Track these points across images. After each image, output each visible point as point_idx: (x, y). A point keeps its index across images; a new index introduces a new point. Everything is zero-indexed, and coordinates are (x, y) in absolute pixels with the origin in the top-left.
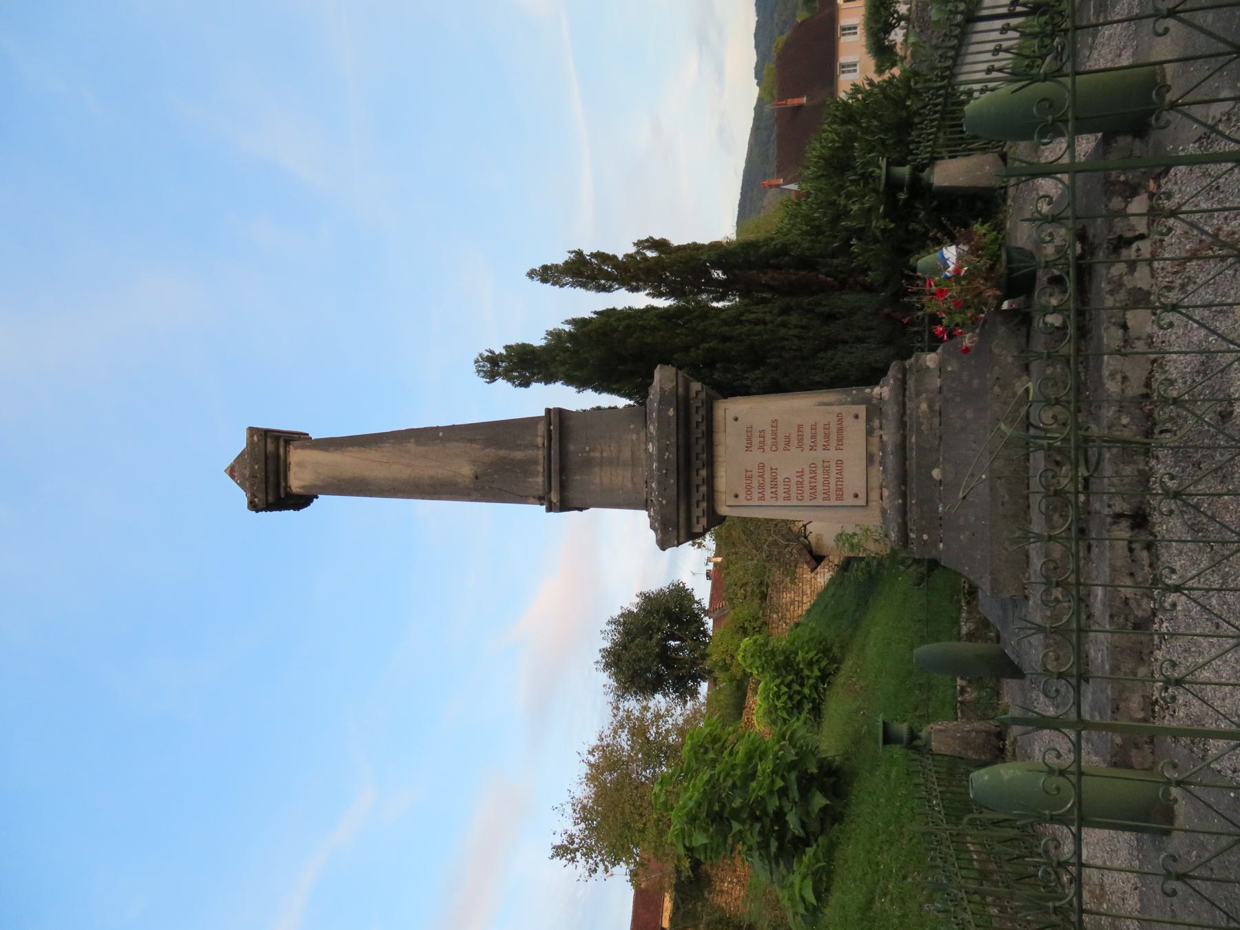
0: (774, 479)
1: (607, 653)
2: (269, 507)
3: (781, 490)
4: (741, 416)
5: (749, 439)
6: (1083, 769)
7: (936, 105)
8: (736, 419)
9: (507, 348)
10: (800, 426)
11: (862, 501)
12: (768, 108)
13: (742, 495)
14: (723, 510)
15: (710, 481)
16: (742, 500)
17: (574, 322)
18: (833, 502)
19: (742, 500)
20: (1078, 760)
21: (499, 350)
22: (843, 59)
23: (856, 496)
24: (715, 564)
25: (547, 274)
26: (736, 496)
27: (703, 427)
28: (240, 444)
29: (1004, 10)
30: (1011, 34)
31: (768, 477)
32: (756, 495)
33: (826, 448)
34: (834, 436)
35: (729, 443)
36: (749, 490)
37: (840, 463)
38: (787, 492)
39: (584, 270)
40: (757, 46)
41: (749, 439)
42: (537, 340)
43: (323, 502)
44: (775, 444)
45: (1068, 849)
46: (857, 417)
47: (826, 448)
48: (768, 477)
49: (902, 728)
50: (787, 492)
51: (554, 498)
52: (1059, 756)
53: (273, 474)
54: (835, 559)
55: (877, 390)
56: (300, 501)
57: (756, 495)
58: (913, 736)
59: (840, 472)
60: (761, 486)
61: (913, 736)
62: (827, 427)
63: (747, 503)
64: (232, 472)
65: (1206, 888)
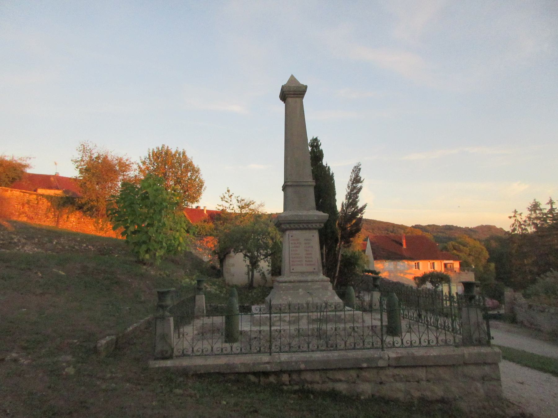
0: (297, 247)
1: (167, 153)
3: (294, 249)
4: (314, 237)
5: (307, 240)
9: (322, 151)
11: (292, 271)
12: (429, 236)
15: (296, 229)
16: (290, 238)
17: (333, 174)
19: (290, 238)
21: (321, 148)
22: (421, 263)
24: (203, 210)
25: (357, 170)
28: (302, 82)
31: (297, 245)
33: (306, 261)
34: (309, 263)
35: (306, 234)
36: (293, 240)
37: (302, 265)
39: (356, 180)
40: (429, 226)
41: (307, 240)
42: (325, 161)
43: (282, 105)
53: (292, 94)
55: (322, 274)
57: (292, 242)
65: (194, 344)
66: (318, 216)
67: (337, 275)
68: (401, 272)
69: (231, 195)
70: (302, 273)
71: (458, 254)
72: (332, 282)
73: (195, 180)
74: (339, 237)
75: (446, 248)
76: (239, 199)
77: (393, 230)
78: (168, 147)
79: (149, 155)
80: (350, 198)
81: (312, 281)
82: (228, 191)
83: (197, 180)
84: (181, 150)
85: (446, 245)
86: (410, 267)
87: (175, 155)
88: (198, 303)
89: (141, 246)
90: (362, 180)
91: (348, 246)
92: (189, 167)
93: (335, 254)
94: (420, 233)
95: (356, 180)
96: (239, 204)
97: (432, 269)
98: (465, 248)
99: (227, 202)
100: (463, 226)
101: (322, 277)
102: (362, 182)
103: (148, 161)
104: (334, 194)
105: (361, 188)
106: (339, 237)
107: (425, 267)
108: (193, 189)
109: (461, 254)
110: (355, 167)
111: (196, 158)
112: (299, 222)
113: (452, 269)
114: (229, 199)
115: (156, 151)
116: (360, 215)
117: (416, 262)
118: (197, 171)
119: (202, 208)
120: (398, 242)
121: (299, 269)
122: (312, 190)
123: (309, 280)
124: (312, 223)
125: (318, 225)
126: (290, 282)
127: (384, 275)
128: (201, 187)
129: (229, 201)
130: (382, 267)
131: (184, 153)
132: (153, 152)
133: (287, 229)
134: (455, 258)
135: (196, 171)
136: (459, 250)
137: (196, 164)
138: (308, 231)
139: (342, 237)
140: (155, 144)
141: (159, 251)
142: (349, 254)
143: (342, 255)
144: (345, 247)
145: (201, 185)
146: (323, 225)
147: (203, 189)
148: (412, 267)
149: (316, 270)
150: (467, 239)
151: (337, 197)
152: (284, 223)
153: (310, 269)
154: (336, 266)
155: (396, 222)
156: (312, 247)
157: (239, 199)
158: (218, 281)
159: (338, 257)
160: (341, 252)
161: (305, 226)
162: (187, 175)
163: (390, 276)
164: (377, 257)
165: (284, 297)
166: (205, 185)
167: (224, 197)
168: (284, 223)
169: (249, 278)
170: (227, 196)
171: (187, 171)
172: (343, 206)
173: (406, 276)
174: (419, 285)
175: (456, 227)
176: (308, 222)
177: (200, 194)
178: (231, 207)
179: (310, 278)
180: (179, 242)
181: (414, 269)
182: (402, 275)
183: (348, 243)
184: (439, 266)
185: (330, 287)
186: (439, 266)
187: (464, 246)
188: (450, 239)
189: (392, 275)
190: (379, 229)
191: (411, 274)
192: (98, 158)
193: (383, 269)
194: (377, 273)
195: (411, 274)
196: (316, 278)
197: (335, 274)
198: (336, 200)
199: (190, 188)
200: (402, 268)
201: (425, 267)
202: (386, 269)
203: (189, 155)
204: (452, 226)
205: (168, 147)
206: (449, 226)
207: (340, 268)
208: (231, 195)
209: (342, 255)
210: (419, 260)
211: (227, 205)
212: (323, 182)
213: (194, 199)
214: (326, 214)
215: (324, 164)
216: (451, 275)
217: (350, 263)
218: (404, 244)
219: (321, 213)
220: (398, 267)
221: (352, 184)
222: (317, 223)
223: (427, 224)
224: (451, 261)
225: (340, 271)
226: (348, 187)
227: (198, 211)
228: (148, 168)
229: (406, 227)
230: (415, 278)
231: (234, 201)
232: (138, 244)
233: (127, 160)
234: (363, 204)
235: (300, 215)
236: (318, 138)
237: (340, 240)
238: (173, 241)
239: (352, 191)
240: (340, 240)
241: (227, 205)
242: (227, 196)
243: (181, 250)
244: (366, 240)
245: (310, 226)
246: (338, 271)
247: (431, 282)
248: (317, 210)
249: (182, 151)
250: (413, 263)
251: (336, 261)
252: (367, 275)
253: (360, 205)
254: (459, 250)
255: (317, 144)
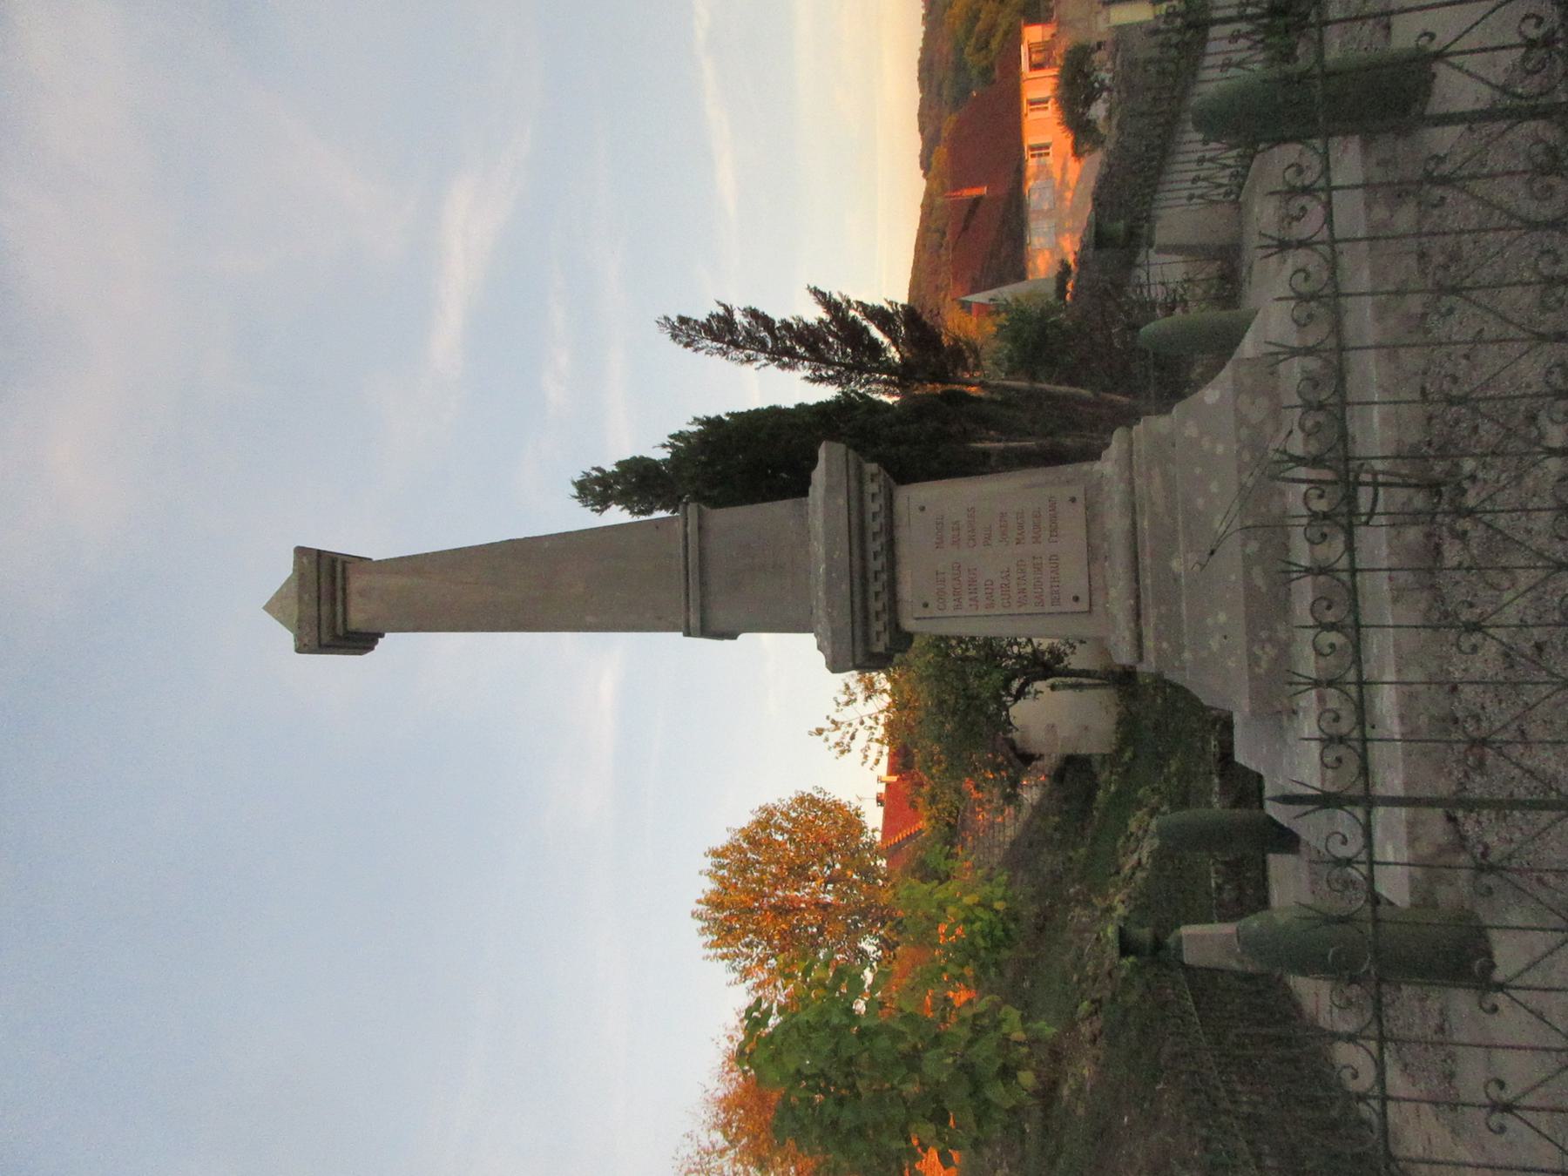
0: (972, 582)
1: (715, 903)
2: (323, 647)
3: (981, 595)
4: (928, 503)
6: (1390, 1092)
7: (1153, 159)
8: (923, 509)
9: (619, 464)
10: (1003, 515)
12: (949, 123)
13: (933, 604)
14: (909, 624)
15: (892, 585)
18: (1048, 608)
20: (1381, 1079)
21: (610, 467)
22: (1030, 139)
23: (1076, 599)
24: (888, 785)
25: (685, 331)
26: (926, 605)
27: (881, 519)
28: (285, 568)
29: (1232, 12)
30: (1243, 43)
31: (964, 578)
32: (950, 604)
37: (1054, 558)
38: (990, 596)
39: (726, 332)
40: (922, 130)
43: (391, 643)
44: (972, 538)
45: (1366, 1080)
46: (1073, 500)
47: (1037, 540)
48: (964, 578)
49: (1145, 934)
50: (990, 596)
51: (694, 621)
52: (1345, 842)
53: (336, 605)
54: (1049, 763)
55: (1097, 466)
56: (361, 642)
58: (1158, 945)
59: (1056, 569)
60: (956, 592)
61: (1158, 945)
62: (1037, 515)
63: (939, 614)
64: (268, 608)
66: (830, 489)
67: (1086, 393)
68: (1060, 197)
69: (833, 722)
70: (1093, 554)
71: (999, 35)
72: (1129, 418)
73: (794, 820)
74: (939, 389)
75: (986, 72)
76: (843, 699)
77: (938, 231)
78: (699, 902)
79: (724, 957)
80: (791, 353)
81: (1133, 509)
82: (820, 732)
83: (794, 815)
84: (708, 863)
85: (974, 72)
86: (1043, 170)
87: (722, 880)
88: (1214, 958)
89: (987, 1101)
90: (721, 311)
91: (975, 352)
92: (758, 836)
93: (1006, 403)
94: (942, 151)
95: (726, 332)
96: (861, 697)
97: (1049, 105)
98: (982, 16)
99: (853, 738)
100: (920, 31)
101: (1107, 466)
102: (729, 310)
103: (742, 963)
104: (775, 411)
105: (753, 314)
106: (939, 389)
107: (1043, 126)
108: (818, 829)
109: (1004, 25)
110: (674, 337)
111: (730, 817)
112: (861, 578)
113: (1046, 47)
114: (844, 728)
115: (710, 938)
116: (852, 313)
117: (1027, 154)
118: (770, 812)
119: (882, 788)
120: (971, 212)
121: (1073, 578)
122: (722, 518)
123: (1125, 523)
124: (862, 513)
125: (872, 488)
126: (1137, 615)
127: (1070, 247)
128: (814, 802)
129: (851, 730)
130: (1047, 254)
131: (715, 854)
132: (713, 945)
133: (895, 626)
134: (1014, 38)
135: (766, 820)
136: (991, 29)
137: (745, 819)
138: (902, 534)
139: (940, 376)
140: (689, 938)
141: (1005, 1028)
142: (1006, 348)
143: (1011, 373)
144: (977, 366)
145: (807, 802)
146: (872, 467)
147: (821, 796)
148: (1045, 166)
149: (1077, 491)
150: (956, 10)
151: (789, 403)
152: (866, 639)
153: (1073, 523)
154: (1050, 396)
155: (915, 224)
156: (971, 511)
157: (843, 699)
158: (1109, 784)
159: (1018, 391)
160: (1000, 378)
161: (875, 546)
162: (780, 844)
163: (1072, 231)
164: (1017, 271)
165: (1214, 644)
166: (808, 790)
167: (837, 744)
168: (866, 639)
169: (1095, 686)
170: (835, 736)
171: (770, 843)
172: (821, 379)
173: (1072, 184)
174: (1099, 142)
175: (924, 50)
176: (859, 532)
177: (839, 806)
178: (869, 722)
179: (1115, 523)
180: (979, 904)
181: (1049, 160)
182: (1069, 195)
183: (962, 354)
184: (1039, 86)
185: (1156, 425)
186: (1039, 86)
187: (977, 18)
188: (960, 67)
189: (1068, 224)
190: (935, 272)
191: (1064, 169)
192: (725, 1127)
193: (1052, 252)
194: (1065, 271)
195: (1064, 169)
196: (1115, 495)
197: (1085, 402)
198: (801, 407)
199: (818, 836)
200: (1048, 194)
201: (1043, 126)
202: (1052, 243)
203: (721, 840)
204: (920, 61)
205: (699, 902)
206: (921, 71)
207: (1058, 383)
208: (833, 722)
209: (1011, 373)
210: (1021, 148)
211: (863, 735)
212: (736, 463)
213: (851, 822)
214: (822, 453)
215: (665, 454)
216: (1065, 43)
217: (1036, 341)
218: (975, 192)
219: (819, 475)
220: (1046, 207)
221: (737, 346)
222: (861, 492)
223: (919, 136)
224: (1024, 50)
225: (1072, 382)
226: (749, 360)
227: (889, 800)
228: (762, 961)
229: (929, 194)
230: (1077, 154)
231: (849, 714)
232: (984, 1111)
233: (731, 1038)
234: (811, 298)
235: (828, 572)
236: (577, 478)
237: (949, 387)
238: (977, 925)
239: (762, 347)
240: (949, 387)
241: (863, 735)
242: (835, 736)
243: (1004, 898)
244: (966, 306)
245: (875, 526)
246: (1073, 390)
247: (1088, 102)
248: (805, 493)
249: (710, 859)
250: (1032, 164)
251: (1030, 396)
252: (1074, 297)
253: (814, 313)
254: (991, 29)
255: (597, 480)
